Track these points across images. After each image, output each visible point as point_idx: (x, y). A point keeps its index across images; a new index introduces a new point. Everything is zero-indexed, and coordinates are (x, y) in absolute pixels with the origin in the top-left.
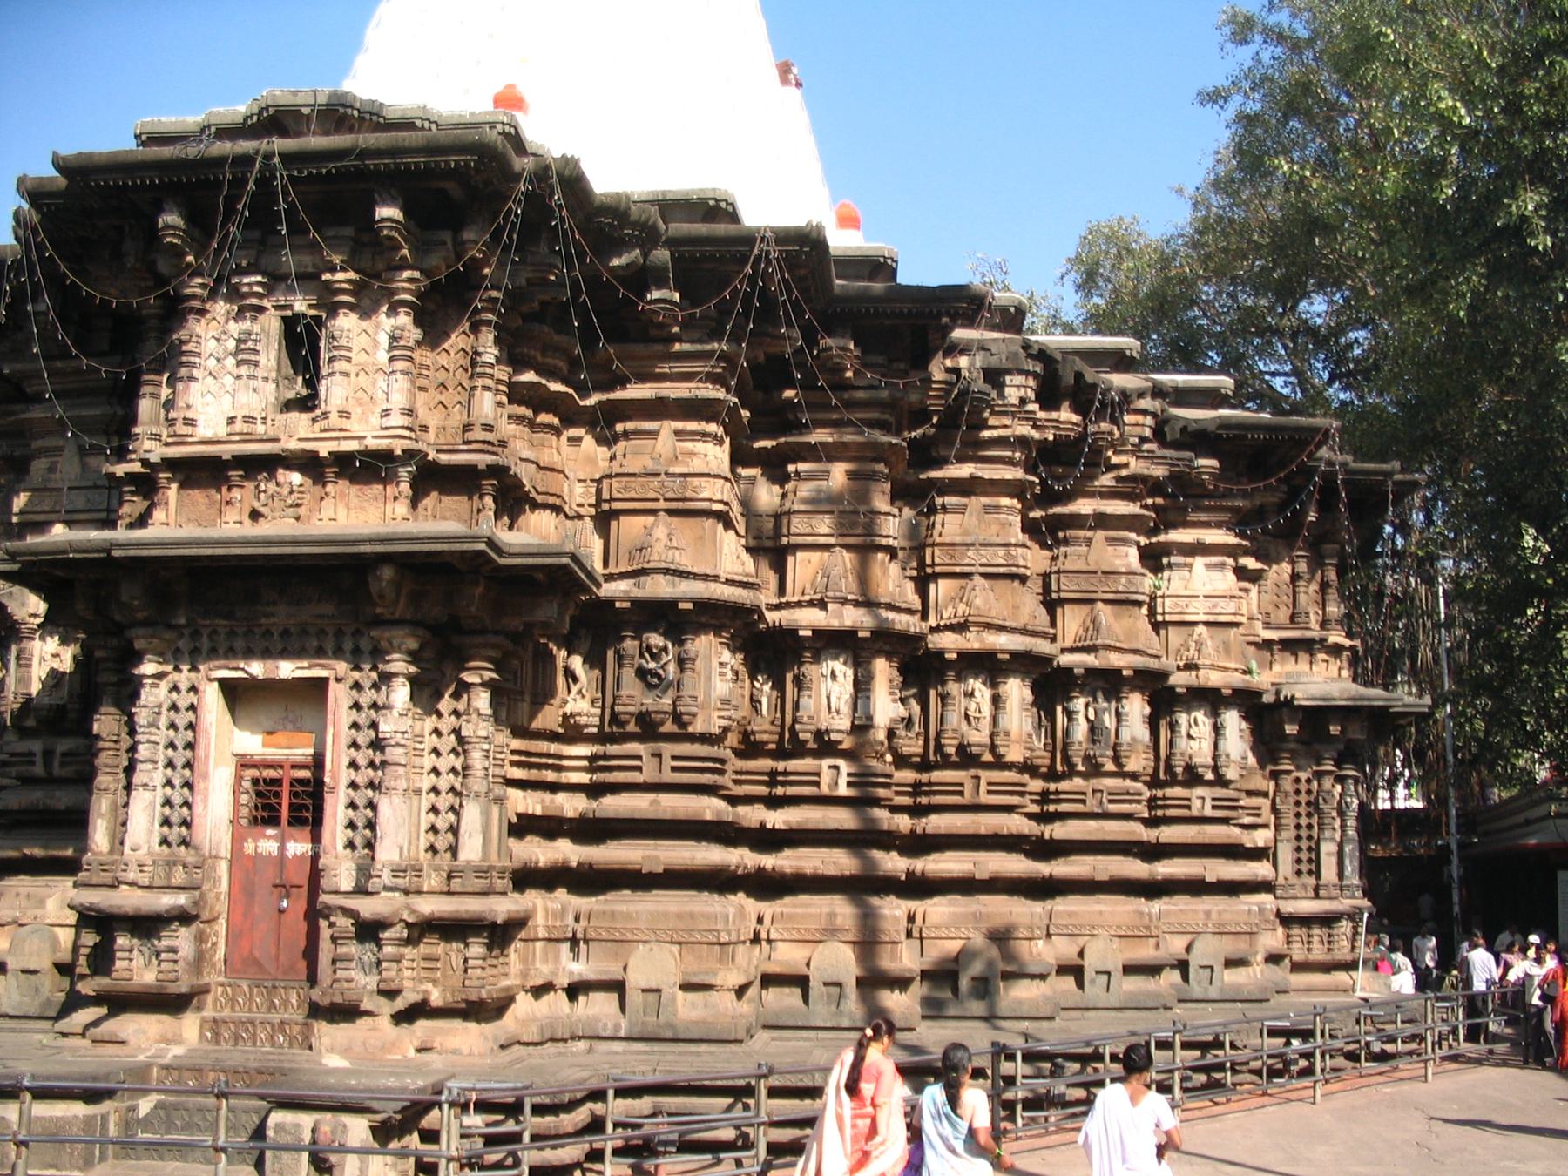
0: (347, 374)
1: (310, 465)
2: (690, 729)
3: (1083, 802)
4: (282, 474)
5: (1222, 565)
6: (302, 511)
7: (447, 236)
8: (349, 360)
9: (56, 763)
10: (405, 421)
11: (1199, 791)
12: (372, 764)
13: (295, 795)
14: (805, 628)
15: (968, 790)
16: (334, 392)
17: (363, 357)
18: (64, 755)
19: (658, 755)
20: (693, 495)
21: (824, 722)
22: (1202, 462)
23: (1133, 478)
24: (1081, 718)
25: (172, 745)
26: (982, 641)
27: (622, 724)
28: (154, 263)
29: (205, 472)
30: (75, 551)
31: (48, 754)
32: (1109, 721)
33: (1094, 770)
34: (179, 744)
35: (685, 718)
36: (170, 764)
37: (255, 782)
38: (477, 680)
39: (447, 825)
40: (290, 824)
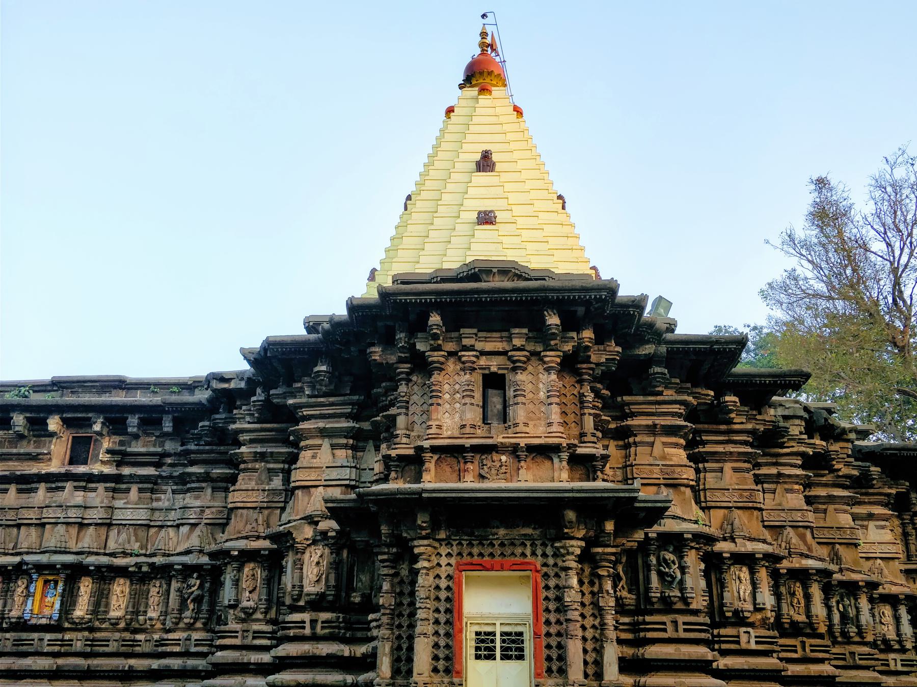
0: (524, 404)
1: (514, 450)
2: (691, 607)
3: (844, 659)
4: (495, 456)
5: (883, 527)
6: (508, 475)
7: (574, 334)
8: (524, 396)
9: (319, 625)
10: (561, 429)
11: (892, 656)
12: (558, 622)
13: (503, 641)
14: (726, 552)
15: (799, 649)
16: (519, 414)
17: (531, 395)
18: (323, 622)
19: (675, 623)
20: (678, 476)
21: (738, 605)
22: (872, 469)
23: (846, 476)
24: (835, 609)
25: (437, 611)
26: (800, 563)
27: (653, 604)
28: (414, 345)
29: (453, 453)
30: (401, 494)
31: (313, 622)
32: (852, 612)
33: (848, 641)
34: (442, 609)
35: (690, 600)
36: (437, 622)
37: (477, 634)
38: (606, 574)
39: (593, 659)
40: (502, 659)
